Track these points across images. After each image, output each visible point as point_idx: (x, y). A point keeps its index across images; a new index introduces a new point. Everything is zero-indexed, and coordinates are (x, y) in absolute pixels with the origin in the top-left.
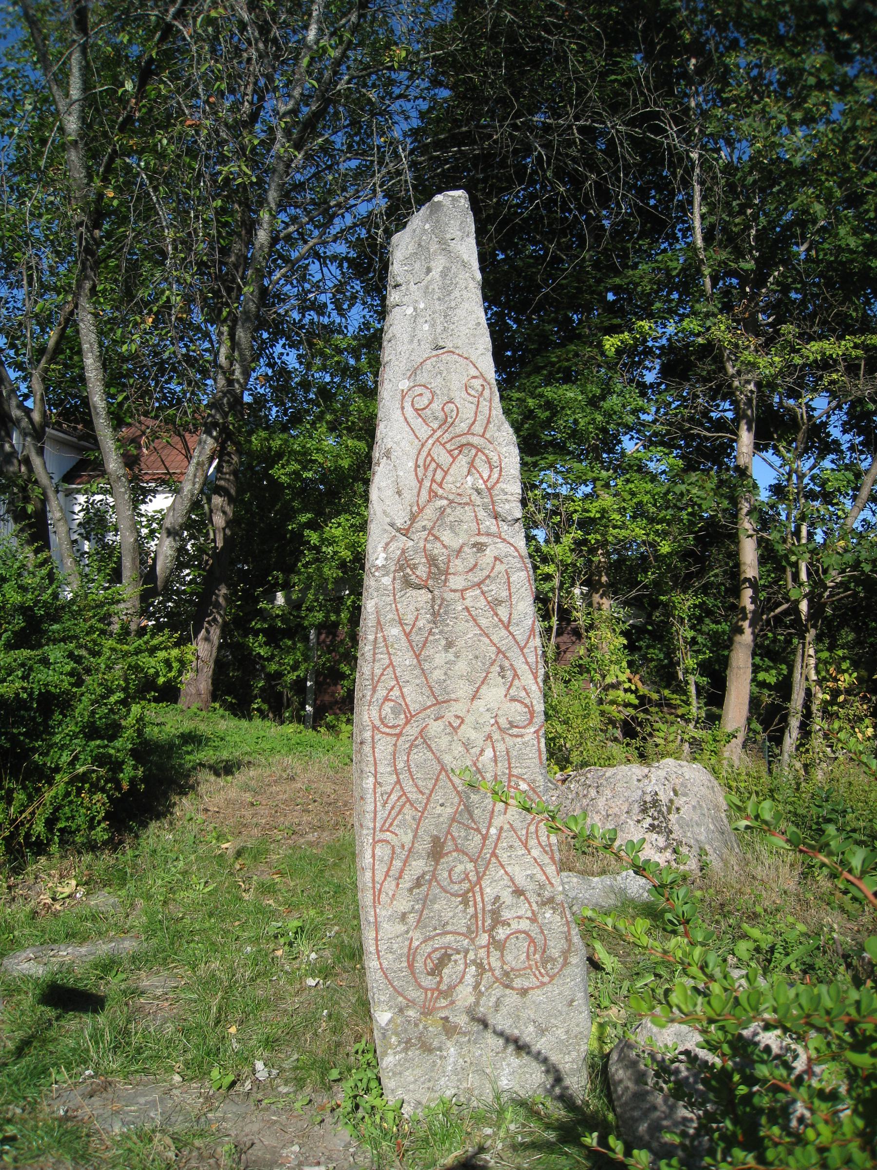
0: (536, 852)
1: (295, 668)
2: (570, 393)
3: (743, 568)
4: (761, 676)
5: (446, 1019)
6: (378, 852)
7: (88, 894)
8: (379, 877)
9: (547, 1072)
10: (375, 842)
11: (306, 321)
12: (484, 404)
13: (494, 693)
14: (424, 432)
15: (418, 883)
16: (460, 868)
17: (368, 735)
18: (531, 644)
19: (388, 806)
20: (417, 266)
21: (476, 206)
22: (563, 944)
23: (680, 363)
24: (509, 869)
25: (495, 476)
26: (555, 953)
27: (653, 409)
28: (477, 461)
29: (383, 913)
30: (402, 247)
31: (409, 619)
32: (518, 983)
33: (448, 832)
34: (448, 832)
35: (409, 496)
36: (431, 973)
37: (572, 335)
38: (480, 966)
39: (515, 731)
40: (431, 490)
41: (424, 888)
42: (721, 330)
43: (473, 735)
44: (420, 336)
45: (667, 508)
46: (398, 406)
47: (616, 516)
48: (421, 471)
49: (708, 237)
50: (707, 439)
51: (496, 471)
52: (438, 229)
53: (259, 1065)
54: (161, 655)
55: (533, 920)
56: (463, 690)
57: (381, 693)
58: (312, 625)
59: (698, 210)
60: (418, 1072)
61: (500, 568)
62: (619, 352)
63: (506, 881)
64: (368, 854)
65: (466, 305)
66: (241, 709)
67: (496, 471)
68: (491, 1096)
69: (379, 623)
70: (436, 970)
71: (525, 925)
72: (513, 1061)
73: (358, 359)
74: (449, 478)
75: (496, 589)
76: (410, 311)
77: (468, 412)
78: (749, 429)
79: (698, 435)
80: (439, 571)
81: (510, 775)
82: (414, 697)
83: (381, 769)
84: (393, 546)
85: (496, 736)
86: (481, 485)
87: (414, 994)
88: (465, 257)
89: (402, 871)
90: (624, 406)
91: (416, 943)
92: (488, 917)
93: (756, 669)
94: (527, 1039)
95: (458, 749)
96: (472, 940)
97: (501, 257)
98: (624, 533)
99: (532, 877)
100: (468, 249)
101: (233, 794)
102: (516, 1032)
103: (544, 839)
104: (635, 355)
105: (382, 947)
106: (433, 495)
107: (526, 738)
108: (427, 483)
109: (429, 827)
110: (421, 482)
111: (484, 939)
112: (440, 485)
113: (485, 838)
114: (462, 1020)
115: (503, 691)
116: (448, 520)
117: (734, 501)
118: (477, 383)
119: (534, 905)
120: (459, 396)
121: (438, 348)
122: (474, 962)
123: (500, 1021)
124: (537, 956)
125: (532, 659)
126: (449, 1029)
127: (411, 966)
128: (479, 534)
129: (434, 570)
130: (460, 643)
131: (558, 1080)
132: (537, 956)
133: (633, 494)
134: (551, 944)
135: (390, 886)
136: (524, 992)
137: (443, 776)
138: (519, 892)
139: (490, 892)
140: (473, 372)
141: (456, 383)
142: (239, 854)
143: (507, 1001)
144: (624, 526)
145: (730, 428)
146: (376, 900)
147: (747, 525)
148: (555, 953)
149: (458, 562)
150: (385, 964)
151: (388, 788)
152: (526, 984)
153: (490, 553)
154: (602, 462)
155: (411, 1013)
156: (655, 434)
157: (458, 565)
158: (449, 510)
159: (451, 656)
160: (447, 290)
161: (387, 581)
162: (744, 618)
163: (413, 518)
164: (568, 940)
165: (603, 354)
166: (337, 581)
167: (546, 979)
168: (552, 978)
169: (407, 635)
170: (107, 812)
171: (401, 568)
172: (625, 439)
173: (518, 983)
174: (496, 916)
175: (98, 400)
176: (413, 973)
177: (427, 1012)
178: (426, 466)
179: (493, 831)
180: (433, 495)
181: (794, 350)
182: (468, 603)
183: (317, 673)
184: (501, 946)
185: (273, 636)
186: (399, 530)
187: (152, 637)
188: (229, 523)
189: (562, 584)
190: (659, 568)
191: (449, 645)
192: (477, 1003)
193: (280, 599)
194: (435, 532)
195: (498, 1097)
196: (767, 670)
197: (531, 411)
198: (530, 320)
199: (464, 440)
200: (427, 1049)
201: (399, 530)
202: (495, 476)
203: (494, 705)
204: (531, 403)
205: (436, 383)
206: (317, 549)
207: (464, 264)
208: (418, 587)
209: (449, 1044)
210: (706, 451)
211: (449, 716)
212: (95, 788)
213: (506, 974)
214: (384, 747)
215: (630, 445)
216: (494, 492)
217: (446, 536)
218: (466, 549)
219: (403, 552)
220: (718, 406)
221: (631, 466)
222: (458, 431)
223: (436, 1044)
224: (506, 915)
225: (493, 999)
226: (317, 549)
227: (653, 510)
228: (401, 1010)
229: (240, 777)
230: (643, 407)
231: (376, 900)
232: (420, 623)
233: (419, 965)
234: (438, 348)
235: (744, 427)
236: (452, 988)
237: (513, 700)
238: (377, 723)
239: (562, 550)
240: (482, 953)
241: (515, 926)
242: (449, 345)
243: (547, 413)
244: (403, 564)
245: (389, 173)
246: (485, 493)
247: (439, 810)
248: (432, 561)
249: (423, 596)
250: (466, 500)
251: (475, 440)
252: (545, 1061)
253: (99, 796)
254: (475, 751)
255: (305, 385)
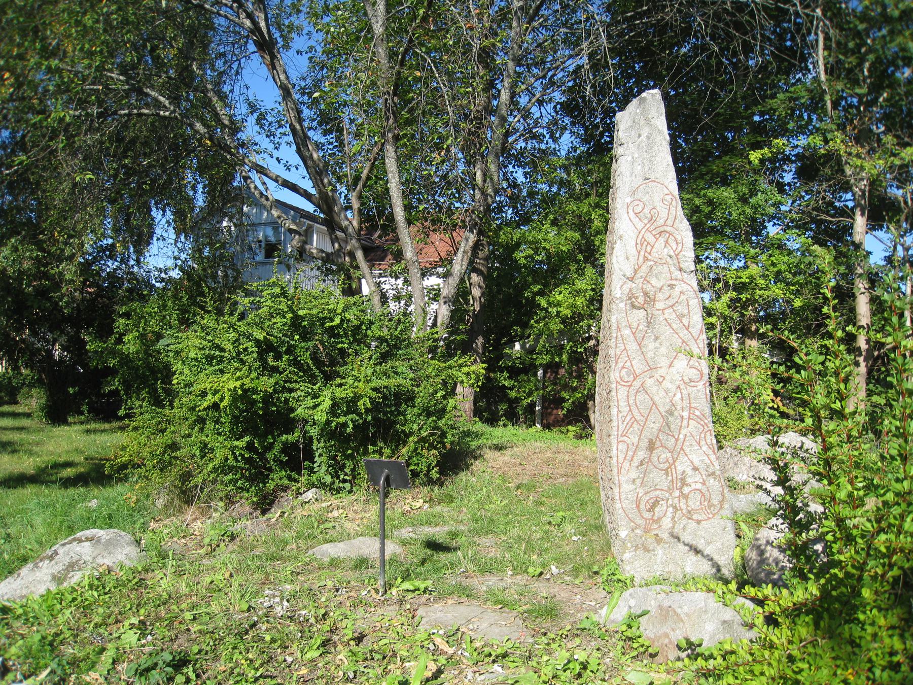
0: (705, 448)
1: (530, 394)
2: (726, 194)
3: (859, 317)
4: (875, 398)
5: (657, 535)
6: (620, 447)
7: (430, 507)
8: (621, 460)
9: (713, 565)
10: (618, 442)
11: (529, 146)
12: (673, 209)
13: (681, 363)
14: (640, 225)
15: (641, 464)
16: (664, 456)
17: (613, 386)
18: (701, 338)
19: (625, 423)
20: (633, 133)
21: (666, 97)
22: (720, 497)
23: (810, 168)
24: (690, 457)
25: (680, 248)
26: (715, 502)
27: (790, 202)
28: (670, 241)
29: (623, 479)
30: (623, 120)
31: (635, 325)
32: (695, 517)
33: (657, 437)
34: (657, 437)
35: (633, 260)
36: (649, 511)
37: (728, 149)
38: (675, 507)
39: (692, 384)
40: (645, 256)
41: (645, 466)
42: (838, 143)
43: (670, 386)
44: (636, 173)
45: (800, 274)
46: (625, 211)
47: (761, 281)
48: (639, 246)
49: (829, 71)
50: (831, 222)
51: (680, 246)
52: (644, 112)
53: (553, 568)
54: (465, 369)
55: (704, 484)
56: (664, 362)
57: (620, 364)
58: (541, 365)
59: (821, 54)
60: (642, 562)
61: (683, 297)
62: (762, 161)
63: (689, 463)
64: (614, 448)
65: (661, 154)
66: (492, 421)
67: (680, 246)
68: (681, 576)
69: (618, 327)
70: (651, 509)
71: (699, 486)
72: (693, 557)
73: (569, 174)
74: (654, 250)
75: (681, 309)
76: (630, 158)
77: (664, 214)
78: (862, 215)
79: (826, 221)
80: (650, 299)
81: (690, 407)
82: (638, 366)
83: (621, 404)
84: (625, 287)
85: (682, 386)
86: (672, 253)
87: (640, 521)
88: (660, 128)
89: (633, 457)
90: (766, 201)
91: (640, 495)
92: (679, 481)
93: (870, 393)
94: (700, 547)
95: (662, 393)
96: (671, 494)
97: (672, 93)
98: (767, 293)
99: (702, 461)
100: (661, 123)
101: (507, 458)
102: (694, 543)
103: (708, 441)
104: (777, 161)
105: (623, 497)
106: (646, 259)
107: (699, 387)
108: (642, 253)
109: (647, 434)
110: (639, 252)
111: (677, 493)
112: (650, 254)
113: (677, 440)
114: (665, 536)
115: (686, 362)
116: (654, 272)
117: (850, 268)
118: (668, 198)
119: (704, 477)
120: (659, 205)
121: (646, 179)
122: (672, 505)
123: (686, 537)
125: (701, 346)
126: (658, 540)
127: (638, 507)
129: (647, 299)
130: (662, 337)
131: (719, 570)
133: (773, 265)
134: (713, 497)
135: (626, 465)
136: (698, 522)
137: (654, 407)
138: (696, 469)
139: (680, 469)
140: (666, 192)
141: (657, 198)
142: (518, 488)
143: (690, 526)
144: (767, 288)
145: (848, 213)
146: (619, 472)
147: (861, 285)
148: (715, 502)
149: (660, 294)
150: (624, 506)
151: (625, 414)
152: (700, 518)
153: (677, 290)
154: (752, 243)
155: (638, 531)
156: (792, 221)
157: (660, 296)
159: (657, 344)
160: (650, 147)
161: (622, 305)
162: (860, 355)
163: (636, 271)
164: (723, 495)
165: (750, 162)
166: (561, 332)
167: (711, 516)
168: (714, 515)
169: (634, 334)
170: (438, 462)
171: (630, 298)
172: (769, 225)
173: (695, 517)
174: (683, 481)
176: (639, 511)
177: (647, 531)
178: (641, 244)
179: (681, 436)
180: (646, 259)
181: (895, 155)
182: (666, 316)
183: (544, 399)
184: (686, 497)
185: (514, 373)
186: (628, 278)
187: (460, 358)
188: (483, 294)
189: (722, 331)
190: (795, 319)
191: (656, 339)
192: (673, 527)
193: (517, 346)
195: (685, 576)
196: (879, 394)
197: (698, 207)
198: (695, 140)
199: (662, 229)
200: (647, 550)
201: (628, 278)
202: (680, 248)
203: (681, 370)
204: (698, 201)
205: (646, 199)
206: (546, 310)
207: (660, 132)
208: (639, 308)
209: (658, 548)
210: (832, 232)
211: (657, 376)
212: (432, 446)
213: (689, 512)
214: (623, 392)
215: (772, 230)
216: (680, 257)
217: (654, 281)
218: (665, 288)
219: (630, 290)
220: (841, 197)
221: (773, 245)
222: (659, 224)
223: (651, 548)
224: (689, 480)
225: (682, 525)
226: (546, 310)
227: (789, 276)
228: (633, 530)
229: (508, 452)
230: (782, 203)
231: (619, 472)
232: (641, 327)
233: (642, 506)
234: (646, 179)
235: (858, 212)
236: (660, 519)
237: (691, 367)
238: (619, 380)
239: (721, 305)
240: (676, 500)
241: (693, 486)
242: (653, 177)
243: (710, 208)
244: (631, 296)
246: (675, 257)
247: (652, 425)
248: (646, 294)
249: (642, 313)
250: (664, 261)
251: (668, 229)
252: (711, 560)
253: (434, 451)
254: (671, 394)
255: (532, 194)
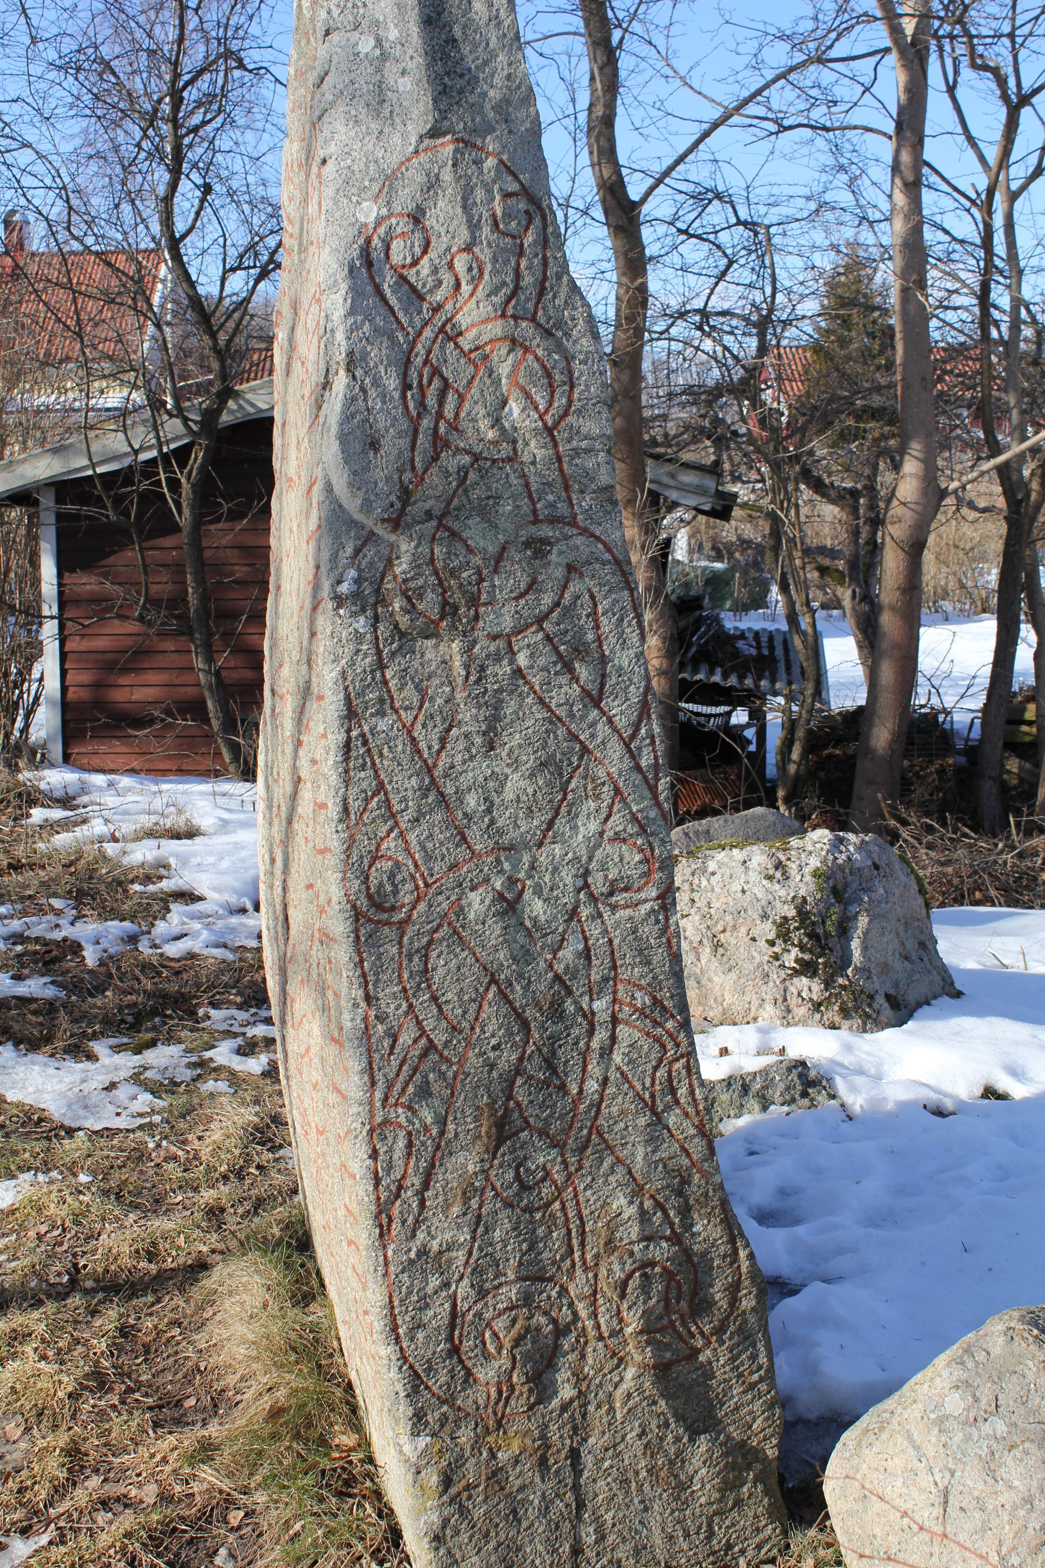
25: (560, 402)
124: (683, 1304)
128: (536, 521)
132: (683, 1304)
158: (472, 476)
175: (49, 630)
194: (449, 522)
245: (485, 511)
